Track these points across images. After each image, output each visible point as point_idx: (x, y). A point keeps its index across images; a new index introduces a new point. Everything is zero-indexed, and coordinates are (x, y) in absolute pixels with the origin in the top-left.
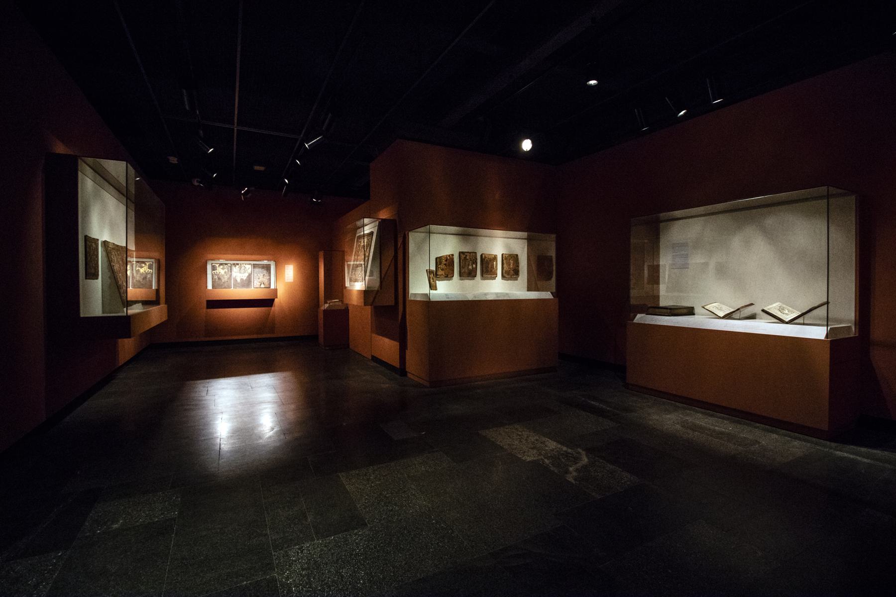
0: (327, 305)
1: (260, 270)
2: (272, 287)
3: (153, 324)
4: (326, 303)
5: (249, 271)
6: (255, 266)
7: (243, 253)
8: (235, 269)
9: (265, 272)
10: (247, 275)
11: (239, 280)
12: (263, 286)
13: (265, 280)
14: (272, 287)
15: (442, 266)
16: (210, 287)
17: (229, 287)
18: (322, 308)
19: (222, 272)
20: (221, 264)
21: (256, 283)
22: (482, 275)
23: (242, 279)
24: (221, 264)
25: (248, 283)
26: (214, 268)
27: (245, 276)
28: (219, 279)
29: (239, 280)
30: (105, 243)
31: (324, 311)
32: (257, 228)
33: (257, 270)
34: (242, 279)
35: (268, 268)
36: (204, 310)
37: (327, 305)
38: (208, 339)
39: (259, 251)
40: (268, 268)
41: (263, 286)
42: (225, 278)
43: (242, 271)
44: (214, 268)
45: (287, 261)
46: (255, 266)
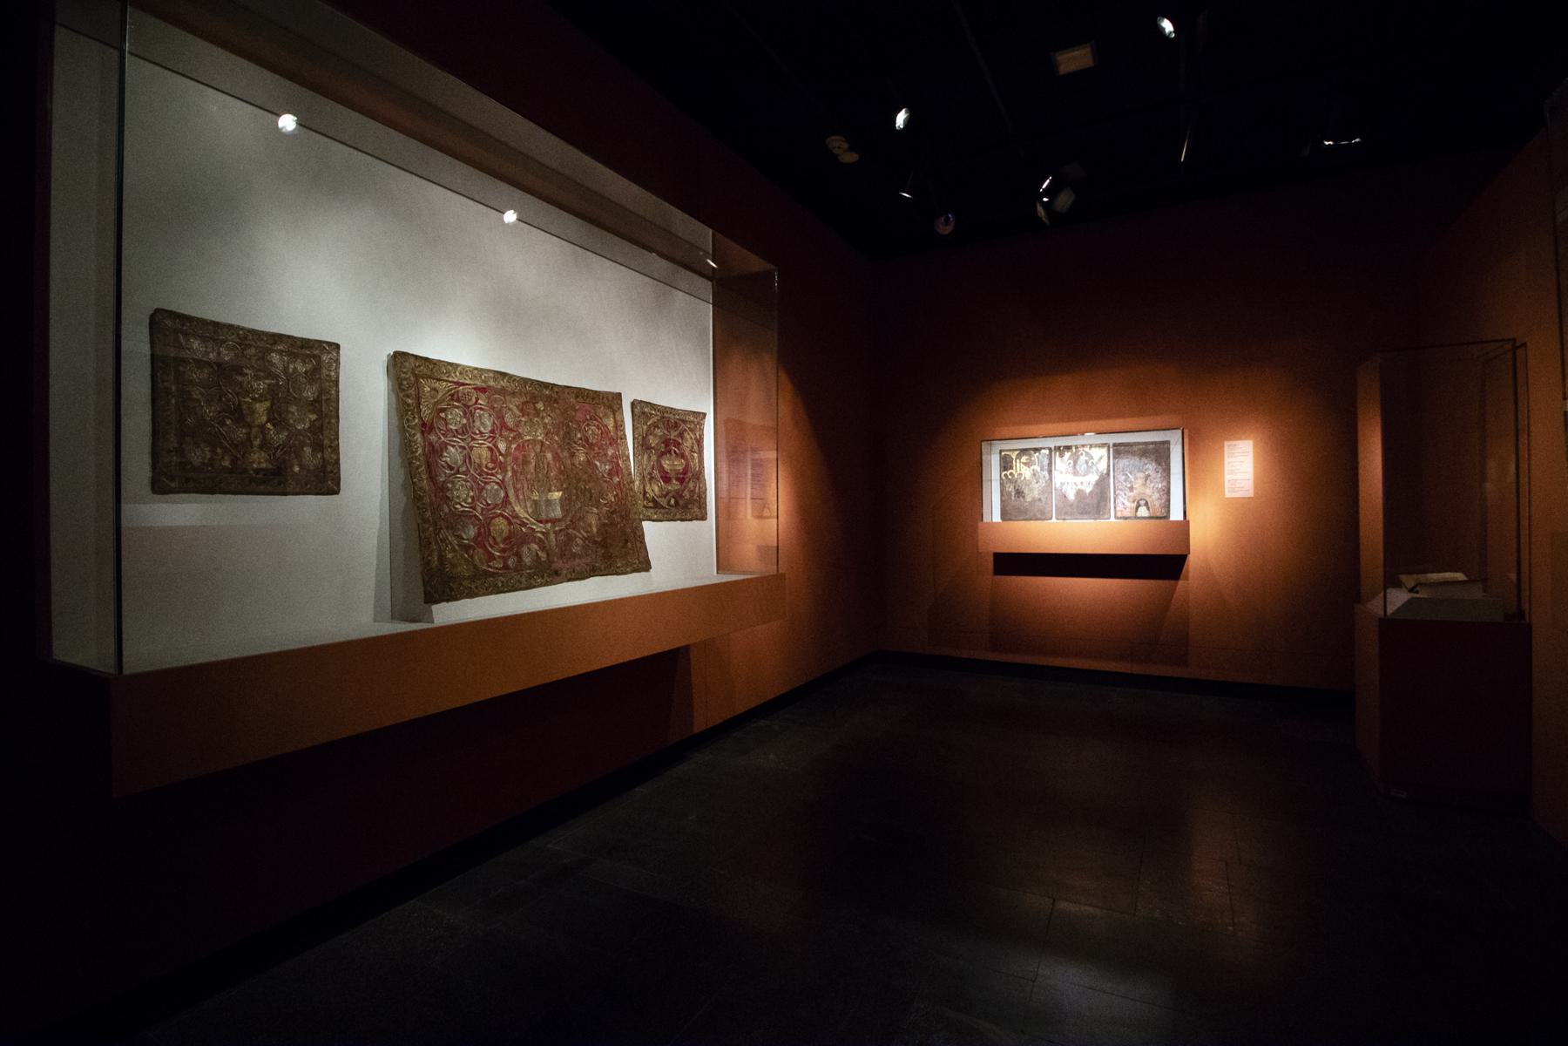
0: (1398, 598)
1: (1135, 461)
2: (1176, 515)
3: (696, 731)
4: (1392, 581)
5: (1103, 466)
6: (1119, 451)
7: (1085, 411)
8: (1062, 464)
9: (1151, 467)
10: (1094, 478)
11: (1071, 496)
12: (1143, 512)
13: (1152, 492)
14: (1176, 515)
15: (675, 485)
16: (993, 512)
17: (1043, 516)
18: (1375, 607)
19: (1026, 473)
20: (1024, 451)
21: (1122, 503)
22: (276, 481)
23: (1079, 493)
24: (1024, 451)
25: (1096, 503)
26: (1006, 464)
27: (1088, 482)
28: (1019, 493)
29: (1071, 496)
30: (408, 372)
31: (1389, 626)
32: (1135, 331)
33: (1124, 462)
34: (1079, 493)
35: (1160, 454)
36: (988, 578)
37: (1398, 598)
38: (992, 656)
39: (1139, 403)
40: (1160, 454)
41: (1143, 512)
42: (1033, 492)
43: (1081, 466)
44: (1006, 464)
45: (1232, 426)
46: (1119, 451)
